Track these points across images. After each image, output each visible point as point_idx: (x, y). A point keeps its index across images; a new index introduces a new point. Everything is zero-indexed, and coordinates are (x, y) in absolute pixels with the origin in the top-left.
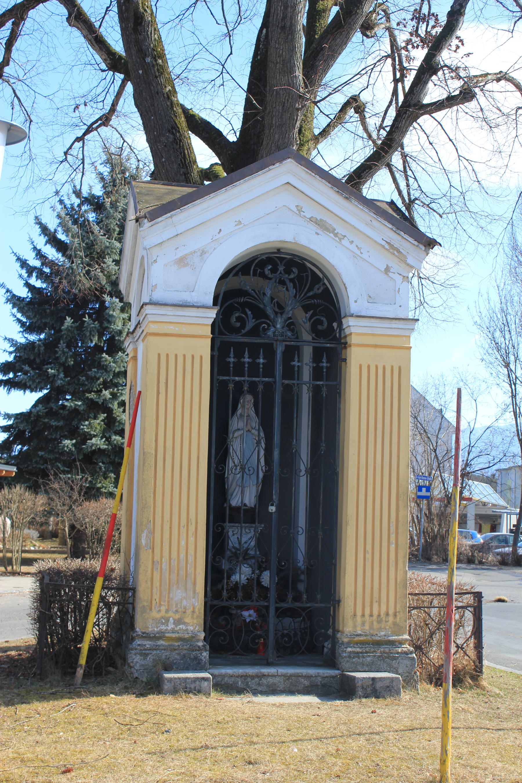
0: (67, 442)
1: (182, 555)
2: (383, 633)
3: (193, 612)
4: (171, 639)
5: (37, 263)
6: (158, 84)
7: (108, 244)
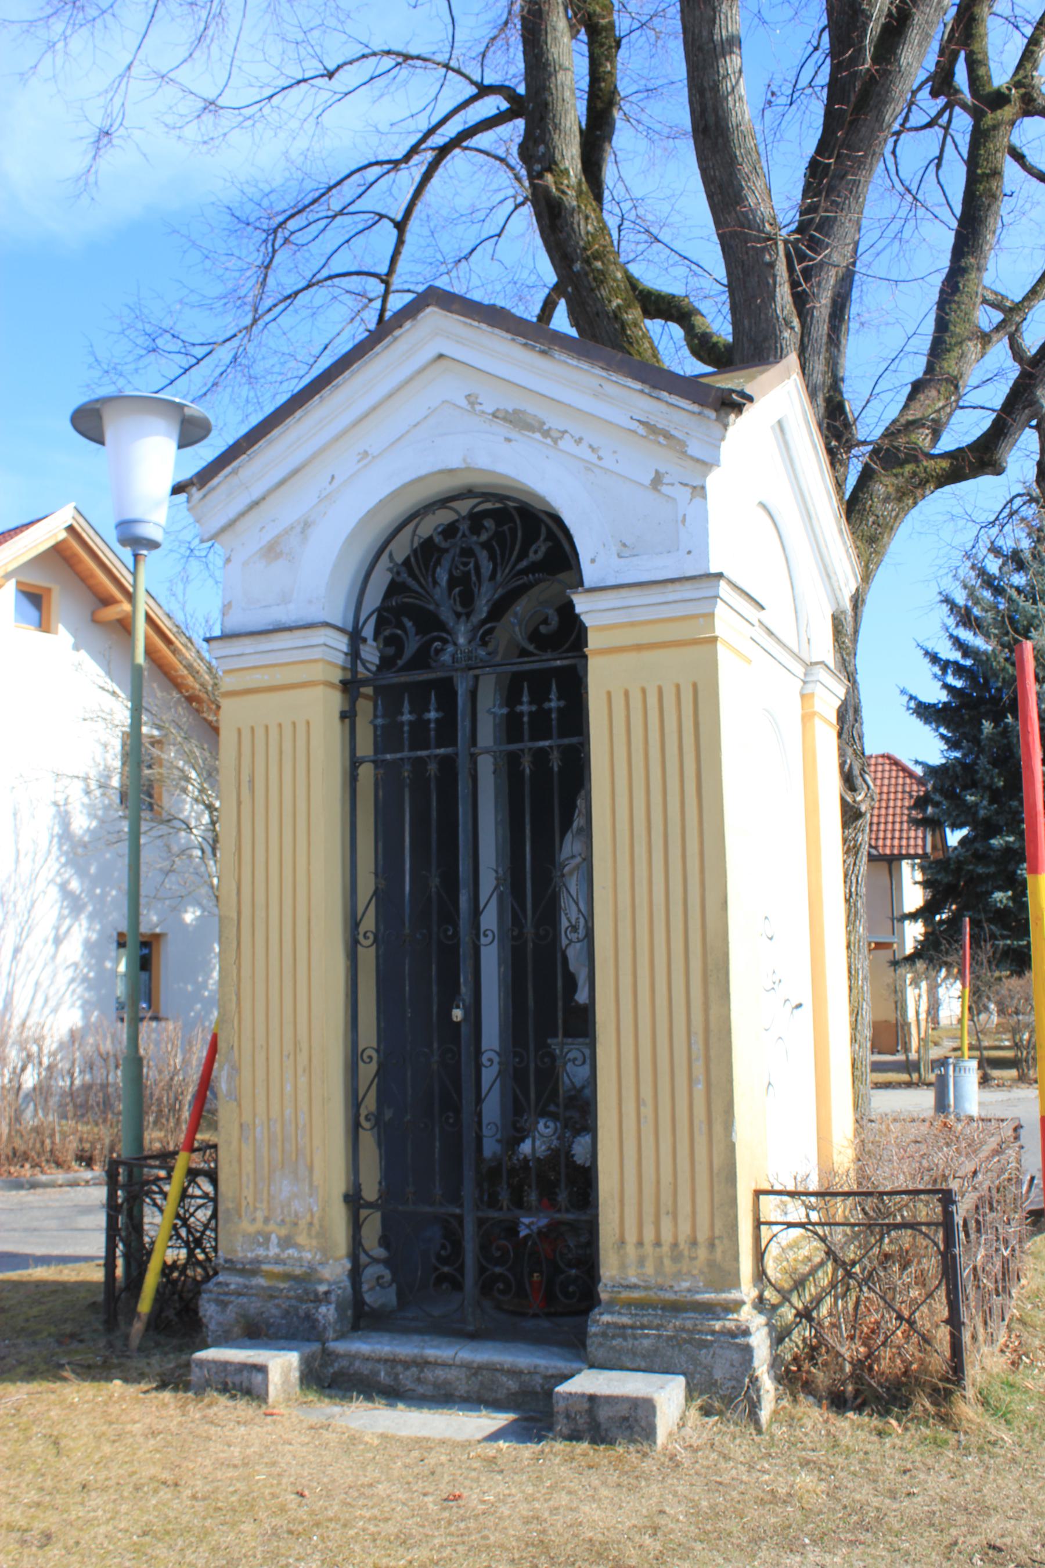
0: (998, 895)
1: (288, 1112)
2: (685, 1285)
3: (311, 1224)
4: (269, 1275)
5: (956, 656)
6: (596, 300)
7: (1033, 612)
